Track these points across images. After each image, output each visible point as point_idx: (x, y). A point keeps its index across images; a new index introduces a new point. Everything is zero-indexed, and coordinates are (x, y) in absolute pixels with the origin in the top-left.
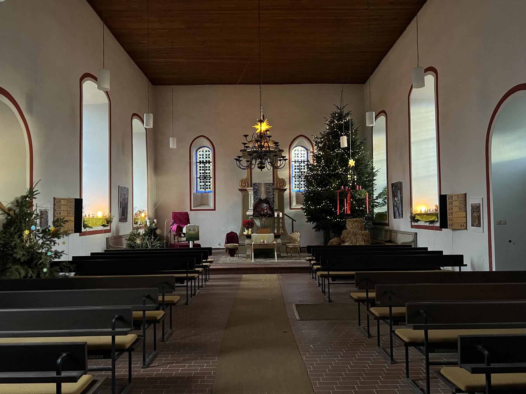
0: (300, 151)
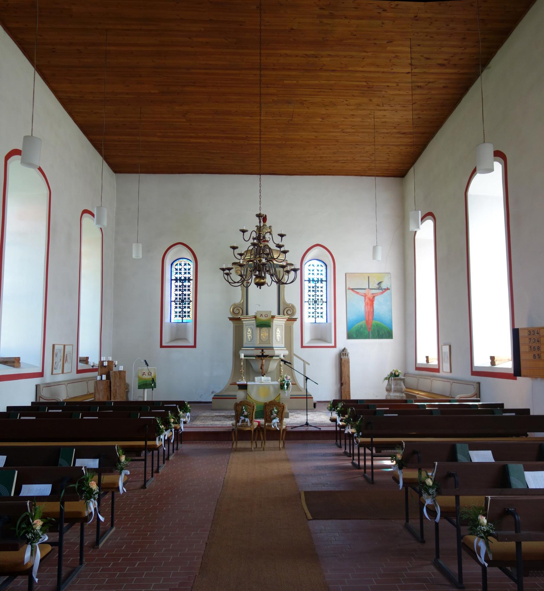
0: (316, 265)
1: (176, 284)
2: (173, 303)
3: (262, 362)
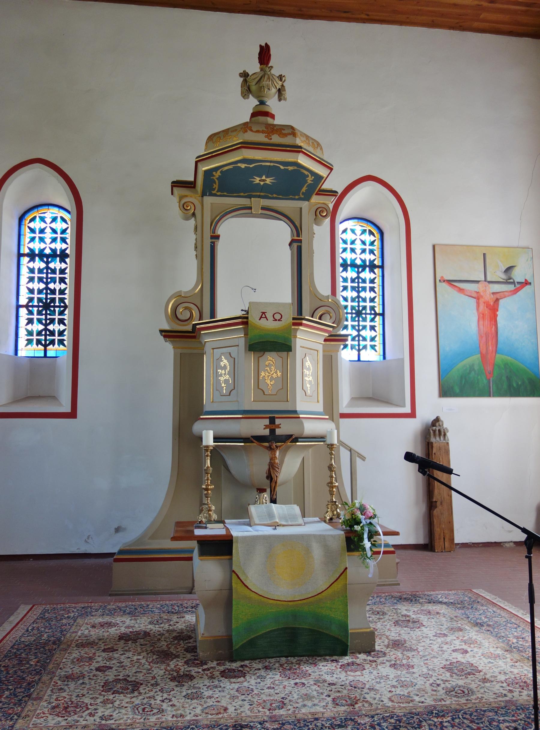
1: (31, 265)
2: (23, 312)
3: (273, 459)
